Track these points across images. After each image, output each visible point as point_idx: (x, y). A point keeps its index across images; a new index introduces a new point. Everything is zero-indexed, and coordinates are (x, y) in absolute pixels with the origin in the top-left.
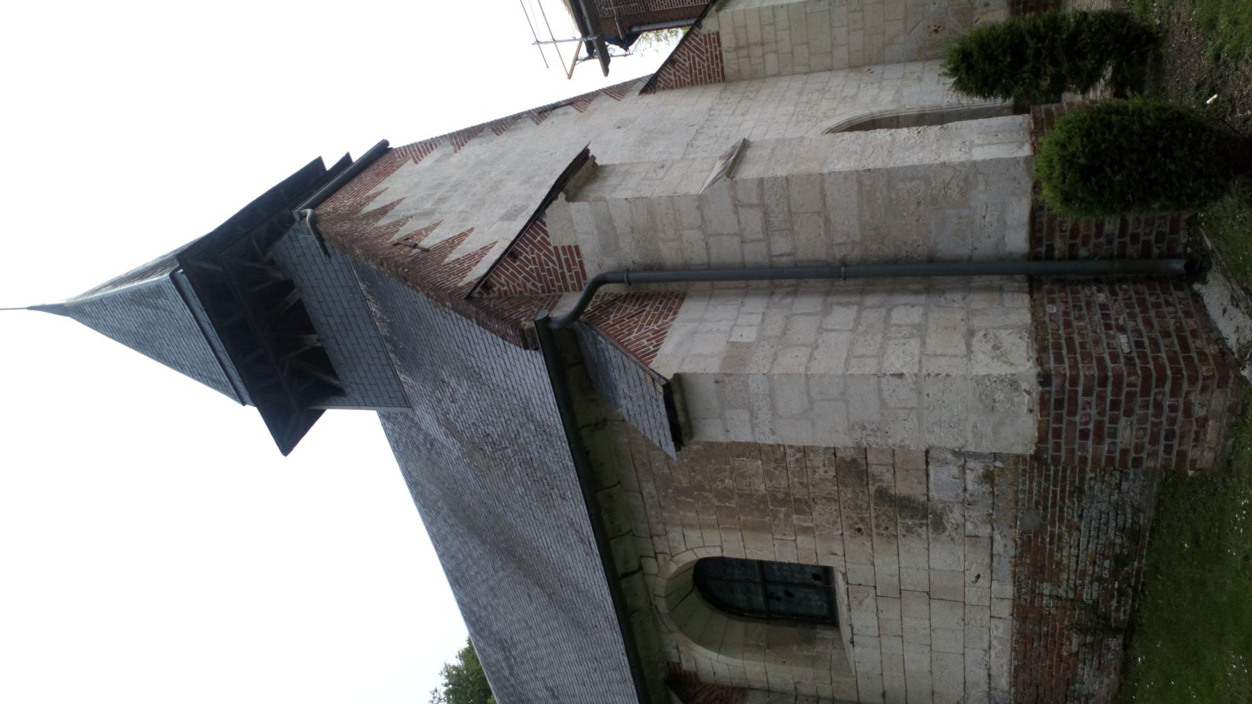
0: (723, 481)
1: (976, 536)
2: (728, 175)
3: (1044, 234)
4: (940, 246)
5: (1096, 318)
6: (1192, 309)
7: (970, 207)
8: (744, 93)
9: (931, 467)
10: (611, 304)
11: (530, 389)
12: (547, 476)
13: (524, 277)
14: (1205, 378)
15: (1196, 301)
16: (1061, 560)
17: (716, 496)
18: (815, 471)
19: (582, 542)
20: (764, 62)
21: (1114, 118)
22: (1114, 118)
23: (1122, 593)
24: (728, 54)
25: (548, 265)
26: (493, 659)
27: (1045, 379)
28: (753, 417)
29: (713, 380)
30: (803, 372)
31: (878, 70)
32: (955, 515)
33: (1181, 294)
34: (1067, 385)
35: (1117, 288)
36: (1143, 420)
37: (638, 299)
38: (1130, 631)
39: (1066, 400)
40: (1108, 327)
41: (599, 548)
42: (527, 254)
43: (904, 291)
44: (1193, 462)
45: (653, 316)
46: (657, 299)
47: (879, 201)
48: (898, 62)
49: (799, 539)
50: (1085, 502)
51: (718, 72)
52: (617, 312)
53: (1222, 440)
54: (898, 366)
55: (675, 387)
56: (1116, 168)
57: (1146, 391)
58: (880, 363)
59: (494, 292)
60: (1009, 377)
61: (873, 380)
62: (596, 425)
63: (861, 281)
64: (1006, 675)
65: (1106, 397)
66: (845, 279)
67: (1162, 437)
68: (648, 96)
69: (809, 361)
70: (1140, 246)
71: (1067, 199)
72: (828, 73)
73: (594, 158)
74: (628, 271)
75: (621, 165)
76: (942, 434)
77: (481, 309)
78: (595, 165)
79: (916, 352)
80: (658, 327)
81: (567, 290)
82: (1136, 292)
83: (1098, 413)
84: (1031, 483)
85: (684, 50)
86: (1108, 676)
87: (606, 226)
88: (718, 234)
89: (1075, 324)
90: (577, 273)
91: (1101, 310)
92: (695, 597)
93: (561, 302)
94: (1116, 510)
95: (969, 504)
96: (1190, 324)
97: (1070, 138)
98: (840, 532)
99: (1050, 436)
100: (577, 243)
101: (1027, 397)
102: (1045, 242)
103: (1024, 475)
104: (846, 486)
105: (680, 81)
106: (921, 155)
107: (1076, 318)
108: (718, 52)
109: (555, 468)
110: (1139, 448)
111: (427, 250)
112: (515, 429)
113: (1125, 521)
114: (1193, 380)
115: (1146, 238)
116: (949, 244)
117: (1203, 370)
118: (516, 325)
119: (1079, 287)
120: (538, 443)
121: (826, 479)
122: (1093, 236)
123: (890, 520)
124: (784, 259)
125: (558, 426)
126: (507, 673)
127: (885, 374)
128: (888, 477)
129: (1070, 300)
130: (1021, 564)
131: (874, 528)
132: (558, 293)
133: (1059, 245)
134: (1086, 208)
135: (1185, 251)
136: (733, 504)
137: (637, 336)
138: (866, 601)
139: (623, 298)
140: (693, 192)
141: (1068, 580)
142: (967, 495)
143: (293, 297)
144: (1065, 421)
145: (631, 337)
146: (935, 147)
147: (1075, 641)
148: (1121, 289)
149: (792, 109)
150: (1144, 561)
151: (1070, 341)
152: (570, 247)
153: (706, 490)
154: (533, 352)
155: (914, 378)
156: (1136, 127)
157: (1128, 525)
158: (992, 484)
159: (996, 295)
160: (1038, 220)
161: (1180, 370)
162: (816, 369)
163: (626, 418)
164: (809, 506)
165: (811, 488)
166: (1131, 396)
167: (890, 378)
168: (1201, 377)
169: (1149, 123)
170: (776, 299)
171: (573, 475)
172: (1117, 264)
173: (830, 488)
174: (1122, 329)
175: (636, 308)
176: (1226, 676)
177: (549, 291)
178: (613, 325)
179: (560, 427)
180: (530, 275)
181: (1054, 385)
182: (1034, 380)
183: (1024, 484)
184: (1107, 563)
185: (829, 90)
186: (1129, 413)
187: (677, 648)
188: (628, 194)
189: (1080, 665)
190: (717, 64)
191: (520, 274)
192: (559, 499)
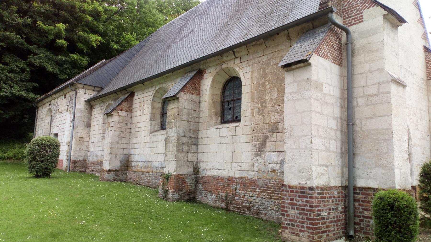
0: (269, 84)
1: (254, 167)
2: (393, 80)
3: (364, 192)
4: (360, 157)
5: (333, 206)
6: (336, 236)
7: (375, 167)
8: (422, 88)
9: (276, 153)
10: (338, 37)
11: (302, 9)
12: (268, 20)
14: (313, 237)
15: (339, 237)
16: (248, 191)
17: (263, 82)
18: (273, 116)
19: (244, 36)
21: (413, 216)
22: (413, 216)
25: (355, 10)
26: (200, 9)
27: (311, 189)
28: (295, 93)
29: (308, 77)
30: (312, 110)
32: (260, 160)
33: (341, 233)
34: (310, 195)
35: (343, 214)
36: (298, 217)
37: (340, 48)
38: (227, 210)
39: (304, 195)
40: (330, 210)
41: (243, 42)
43: (342, 145)
44: (284, 231)
45: (333, 54)
46: (340, 55)
47: (379, 136)
50: (268, 199)
52: (335, 40)
53: (292, 240)
54: (315, 142)
55: (306, 63)
56: (393, 215)
57: (308, 219)
58: (316, 136)
60: (312, 178)
61: (310, 134)
62: (289, 36)
63: (346, 130)
64: (211, 174)
65: (305, 207)
66: (347, 125)
67: (292, 223)
68: (423, 49)
69: (316, 112)
70: (359, 222)
71: (381, 199)
73: (401, 26)
74: (352, 43)
75: (398, 37)
76: (290, 156)
78: (398, 26)
79: (319, 148)
80: (329, 56)
81: (344, 19)
82: (342, 220)
83: (300, 204)
84: (273, 183)
86: (213, 203)
87: (372, 32)
88: (367, 77)
89: (331, 200)
90: (351, 22)
91: (336, 208)
92: (227, 77)
93: (339, 17)
94: (265, 208)
95: (264, 165)
96: (331, 234)
97: (406, 201)
98: (253, 124)
99: (291, 189)
100: (364, 21)
101: (305, 183)
102: (360, 192)
103: (275, 181)
104: (269, 126)
106: (397, 151)
107: (332, 200)
109: (271, 23)
110: (288, 216)
112: (286, 5)
113: (261, 211)
114: (312, 233)
115: (362, 224)
116: (359, 161)
117: (316, 237)
119: (343, 202)
120: (281, 15)
121: (271, 119)
122: (362, 207)
124: (355, 103)
125: (288, 21)
126: (196, 15)
128: (272, 139)
129: (339, 198)
130: (246, 179)
131: (254, 135)
132: (342, 16)
133: (360, 197)
134: (377, 204)
135: (356, 236)
136: (260, 88)
137: (326, 49)
138: (230, 133)
139: (340, 42)
140: (385, 66)
142: (267, 164)
144: (296, 194)
145: (325, 46)
146: (400, 156)
148: (343, 215)
150: (249, 215)
151: (325, 197)
153: (265, 79)
154: (318, 8)
155: (311, 147)
156: (409, 222)
157: (260, 211)
158: (271, 172)
159: (340, 175)
160: (369, 190)
161: (315, 230)
162: (313, 115)
163: (292, 47)
164: (261, 114)
165: (268, 114)
166: (306, 215)
167: (310, 139)
168: (313, 236)
169: (411, 227)
170: (339, 100)
171: (269, 29)
172: (352, 214)
173: (268, 121)
174: (329, 214)
176: (219, 235)
177: (343, 12)
178: (329, 39)
179: (288, 22)
181: (309, 191)
182: (311, 185)
183: (272, 181)
184: (248, 204)
185: (421, 120)
186: (300, 213)
187: (211, 72)
188: (385, 41)
189: (216, 195)
192: (260, 25)
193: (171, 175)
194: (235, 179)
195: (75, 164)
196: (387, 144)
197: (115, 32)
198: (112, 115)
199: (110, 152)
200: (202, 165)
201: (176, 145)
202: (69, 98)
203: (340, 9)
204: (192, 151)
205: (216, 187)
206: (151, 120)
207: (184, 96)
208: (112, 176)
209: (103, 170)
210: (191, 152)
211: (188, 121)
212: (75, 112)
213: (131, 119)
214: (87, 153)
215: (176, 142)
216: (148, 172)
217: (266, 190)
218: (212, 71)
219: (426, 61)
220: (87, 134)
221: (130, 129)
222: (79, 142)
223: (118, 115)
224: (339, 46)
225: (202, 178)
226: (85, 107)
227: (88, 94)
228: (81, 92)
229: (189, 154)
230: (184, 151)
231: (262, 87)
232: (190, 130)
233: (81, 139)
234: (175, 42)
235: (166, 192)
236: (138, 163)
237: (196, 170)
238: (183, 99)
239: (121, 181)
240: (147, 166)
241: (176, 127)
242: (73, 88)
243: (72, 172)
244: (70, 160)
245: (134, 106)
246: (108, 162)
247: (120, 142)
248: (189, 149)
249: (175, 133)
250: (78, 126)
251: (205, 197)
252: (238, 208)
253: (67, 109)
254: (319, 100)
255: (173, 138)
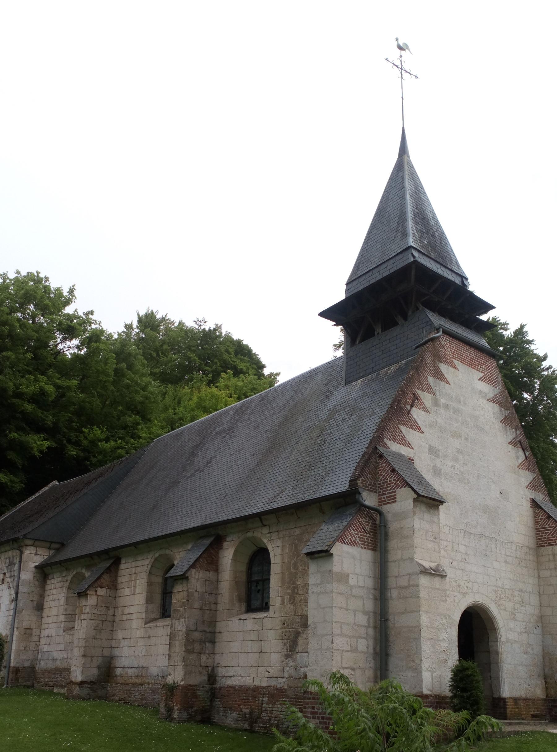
0: (301, 566)
7: (406, 670)
10: (371, 518)
13: (384, 475)
16: (276, 705)
20: (546, 569)
23: (265, 728)
24: (551, 549)
30: (334, 605)
31: (539, 631)
32: (291, 663)
38: (251, 731)
42: (394, 478)
45: (364, 539)
47: (409, 635)
48: (543, 642)
49: (280, 598)
51: (542, 544)
52: (366, 522)
55: (327, 554)
58: (338, 635)
59: (379, 460)
61: (331, 632)
64: (232, 683)
69: (339, 608)
72: (538, 604)
75: (439, 519)
77: (370, 456)
85: (555, 524)
88: (399, 567)
95: (296, 669)
104: (301, 619)
105: (538, 522)
108: (552, 544)
111: (409, 412)
118: (359, 477)
123: (289, 636)
124: (389, 594)
126: (217, 430)
127: (333, 637)
130: (274, 689)
132: (378, 491)
136: (292, 570)
138: (257, 626)
141: (269, 707)
143: (400, 320)
145: (352, 531)
147: (246, 710)
149: (508, 587)
152: (396, 498)
158: (303, 678)
164: (293, 602)
170: (372, 591)
175: (368, 530)
180: (385, 478)
186: (320, 723)
187: (232, 540)
190: (546, 543)
191: (386, 474)
193: (178, 686)
194: (261, 689)
195: (16, 673)
196: (416, 644)
197: (74, 424)
198: (87, 594)
199: (83, 653)
200: (220, 672)
201: (184, 644)
202: (8, 561)
203: (375, 484)
204: (207, 652)
205: (239, 701)
206: (147, 602)
207: (195, 574)
208: (85, 692)
209: (72, 682)
210: (205, 653)
211: (201, 609)
212: (18, 586)
213: (115, 600)
214: (36, 655)
215: (185, 639)
216: (141, 684)
217: (296, 702)
218: (234, 539)
219: (536, 520)
220: (37, 623)
221: (114, 615)
222: (25, 635)
223: (96, 594)
224: (373, 528)
225: (220, 689)
226: (34, 577)
227: (41, 555)
228: (29, 552)
229: (202, 655)
230: (195, 651)
231: (294, 568)
232: (203, 622)
233: (28, 632)
234: (185, 477)
235: (170, 710)
236: (126, 670)
237: (212, 678)
238: (194, 578)
239: (100, 698)
240: (140, 674)
241: (185, 618)
242: (16, 545)
243: (11, 687)
244: (9, 667)
245: (120, 580)
246: (80, 669)
247: (98, 637)
248: (202, 649)
249: (183, 626)
250: (23, 609)
251: (224, 717)
252: (264, 727)
253: (3, 579)
254: (343, 594)
255: (181, 633)
